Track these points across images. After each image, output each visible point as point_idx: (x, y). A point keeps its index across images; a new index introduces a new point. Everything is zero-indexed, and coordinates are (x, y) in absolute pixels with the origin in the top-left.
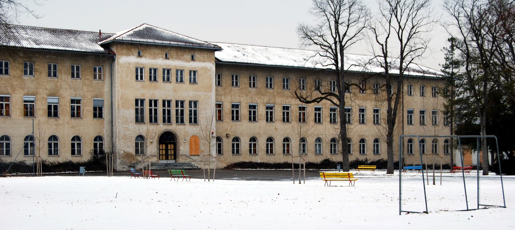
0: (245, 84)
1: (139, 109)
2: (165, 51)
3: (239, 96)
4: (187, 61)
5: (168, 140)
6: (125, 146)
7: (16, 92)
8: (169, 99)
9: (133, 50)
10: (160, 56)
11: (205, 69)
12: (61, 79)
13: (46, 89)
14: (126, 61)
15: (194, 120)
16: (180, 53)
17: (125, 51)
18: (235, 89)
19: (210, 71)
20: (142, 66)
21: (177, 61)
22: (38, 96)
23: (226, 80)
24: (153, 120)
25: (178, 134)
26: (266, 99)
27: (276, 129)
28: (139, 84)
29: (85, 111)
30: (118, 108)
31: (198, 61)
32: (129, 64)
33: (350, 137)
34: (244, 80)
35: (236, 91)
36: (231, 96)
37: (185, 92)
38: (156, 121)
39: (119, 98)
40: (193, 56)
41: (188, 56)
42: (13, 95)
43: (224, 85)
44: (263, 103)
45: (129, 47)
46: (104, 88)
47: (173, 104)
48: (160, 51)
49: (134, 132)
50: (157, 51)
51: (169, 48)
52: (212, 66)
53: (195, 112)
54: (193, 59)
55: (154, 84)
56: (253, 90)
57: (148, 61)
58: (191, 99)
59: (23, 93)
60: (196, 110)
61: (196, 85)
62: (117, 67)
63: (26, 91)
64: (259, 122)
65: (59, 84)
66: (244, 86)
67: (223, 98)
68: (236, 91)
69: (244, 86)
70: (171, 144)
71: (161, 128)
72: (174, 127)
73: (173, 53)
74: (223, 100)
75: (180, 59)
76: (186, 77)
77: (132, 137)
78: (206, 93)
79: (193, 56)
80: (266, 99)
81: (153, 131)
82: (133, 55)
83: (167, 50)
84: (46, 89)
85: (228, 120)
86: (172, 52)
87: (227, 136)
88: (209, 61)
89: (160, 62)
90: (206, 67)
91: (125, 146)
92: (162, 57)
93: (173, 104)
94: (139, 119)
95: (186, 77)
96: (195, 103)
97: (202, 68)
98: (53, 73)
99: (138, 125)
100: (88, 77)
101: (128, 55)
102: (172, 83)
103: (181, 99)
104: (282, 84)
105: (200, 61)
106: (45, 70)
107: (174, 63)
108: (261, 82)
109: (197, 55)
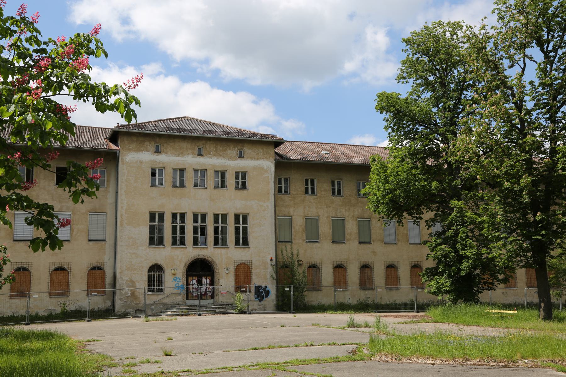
0: (325, 190)
2: (198, 144)
3: (316, 208)
4: (232, 158)
5: (200, 269)
8: (203, 211)
9: (147, 143)
10: (190, 151)
11: (260, 169)
14: (136, 160)
15: (242, 240)
16: (220, 148)
17: (133, 145)
18: (310, 198)
19: (266, 171)
20: (161, 166)
21: (216, 158)
23: (296, 184)
24: (179, 241)
25: (217, 262)
26: (357, 212)
27: (374, 253)
28: (155, 191)
29: (75, 230)
31: (248, 158)
32: (141, 162)
34: (323, 186)
35: (312, 201)
36: (305, 207)
37: (230, 202)
38: (183, 243)
40: (241, 152)
41: (152, 146)
43: (293, 192)
44: (353, 216)
45: (141, 139)
46: (107, 198)
47: (210, 219)
50: (184, 145)
51: (204, 142)
52: (269, 165)
53: (245, 230)
54: (241, 156)
55: (180, 190)
56: (337, 199)
57: (169, 159)
58: (237, 212)
60: (184, 226)
61: (246, 192)
64: (348, 243)
66: (323, 193)
67: (291, 210)
68: (312, 201)
69: (323, 193)
70: (206, 276)
71: (191, 252)
72: (210, 252)
73: (210, 147)
74: (292, 214)
75: (220, 155)
76: (230, 180)
77: (142, 267)
78: (259, 205)
79: (241, 152)
80: (357, 212)
81: (175, 260)
82: (148, 150)
83: (200, 144)
85: (300, 241)
86: (208, 146)
88: (266, 158)
89: (189, 160)
90: (262, 166)
92: (193, 153)
93: (210, 219)
94: (155, 240)
95: (230, 180)
96: (245, 218)
97: (255, 168)
99: (152, 249)
101: (138, 150)
102: (208, 190)
103: (220, 211)
104: (330, 188)
106: (327, 186)
107: (212, 161)
108: (348, 188)
109: (247, 150)
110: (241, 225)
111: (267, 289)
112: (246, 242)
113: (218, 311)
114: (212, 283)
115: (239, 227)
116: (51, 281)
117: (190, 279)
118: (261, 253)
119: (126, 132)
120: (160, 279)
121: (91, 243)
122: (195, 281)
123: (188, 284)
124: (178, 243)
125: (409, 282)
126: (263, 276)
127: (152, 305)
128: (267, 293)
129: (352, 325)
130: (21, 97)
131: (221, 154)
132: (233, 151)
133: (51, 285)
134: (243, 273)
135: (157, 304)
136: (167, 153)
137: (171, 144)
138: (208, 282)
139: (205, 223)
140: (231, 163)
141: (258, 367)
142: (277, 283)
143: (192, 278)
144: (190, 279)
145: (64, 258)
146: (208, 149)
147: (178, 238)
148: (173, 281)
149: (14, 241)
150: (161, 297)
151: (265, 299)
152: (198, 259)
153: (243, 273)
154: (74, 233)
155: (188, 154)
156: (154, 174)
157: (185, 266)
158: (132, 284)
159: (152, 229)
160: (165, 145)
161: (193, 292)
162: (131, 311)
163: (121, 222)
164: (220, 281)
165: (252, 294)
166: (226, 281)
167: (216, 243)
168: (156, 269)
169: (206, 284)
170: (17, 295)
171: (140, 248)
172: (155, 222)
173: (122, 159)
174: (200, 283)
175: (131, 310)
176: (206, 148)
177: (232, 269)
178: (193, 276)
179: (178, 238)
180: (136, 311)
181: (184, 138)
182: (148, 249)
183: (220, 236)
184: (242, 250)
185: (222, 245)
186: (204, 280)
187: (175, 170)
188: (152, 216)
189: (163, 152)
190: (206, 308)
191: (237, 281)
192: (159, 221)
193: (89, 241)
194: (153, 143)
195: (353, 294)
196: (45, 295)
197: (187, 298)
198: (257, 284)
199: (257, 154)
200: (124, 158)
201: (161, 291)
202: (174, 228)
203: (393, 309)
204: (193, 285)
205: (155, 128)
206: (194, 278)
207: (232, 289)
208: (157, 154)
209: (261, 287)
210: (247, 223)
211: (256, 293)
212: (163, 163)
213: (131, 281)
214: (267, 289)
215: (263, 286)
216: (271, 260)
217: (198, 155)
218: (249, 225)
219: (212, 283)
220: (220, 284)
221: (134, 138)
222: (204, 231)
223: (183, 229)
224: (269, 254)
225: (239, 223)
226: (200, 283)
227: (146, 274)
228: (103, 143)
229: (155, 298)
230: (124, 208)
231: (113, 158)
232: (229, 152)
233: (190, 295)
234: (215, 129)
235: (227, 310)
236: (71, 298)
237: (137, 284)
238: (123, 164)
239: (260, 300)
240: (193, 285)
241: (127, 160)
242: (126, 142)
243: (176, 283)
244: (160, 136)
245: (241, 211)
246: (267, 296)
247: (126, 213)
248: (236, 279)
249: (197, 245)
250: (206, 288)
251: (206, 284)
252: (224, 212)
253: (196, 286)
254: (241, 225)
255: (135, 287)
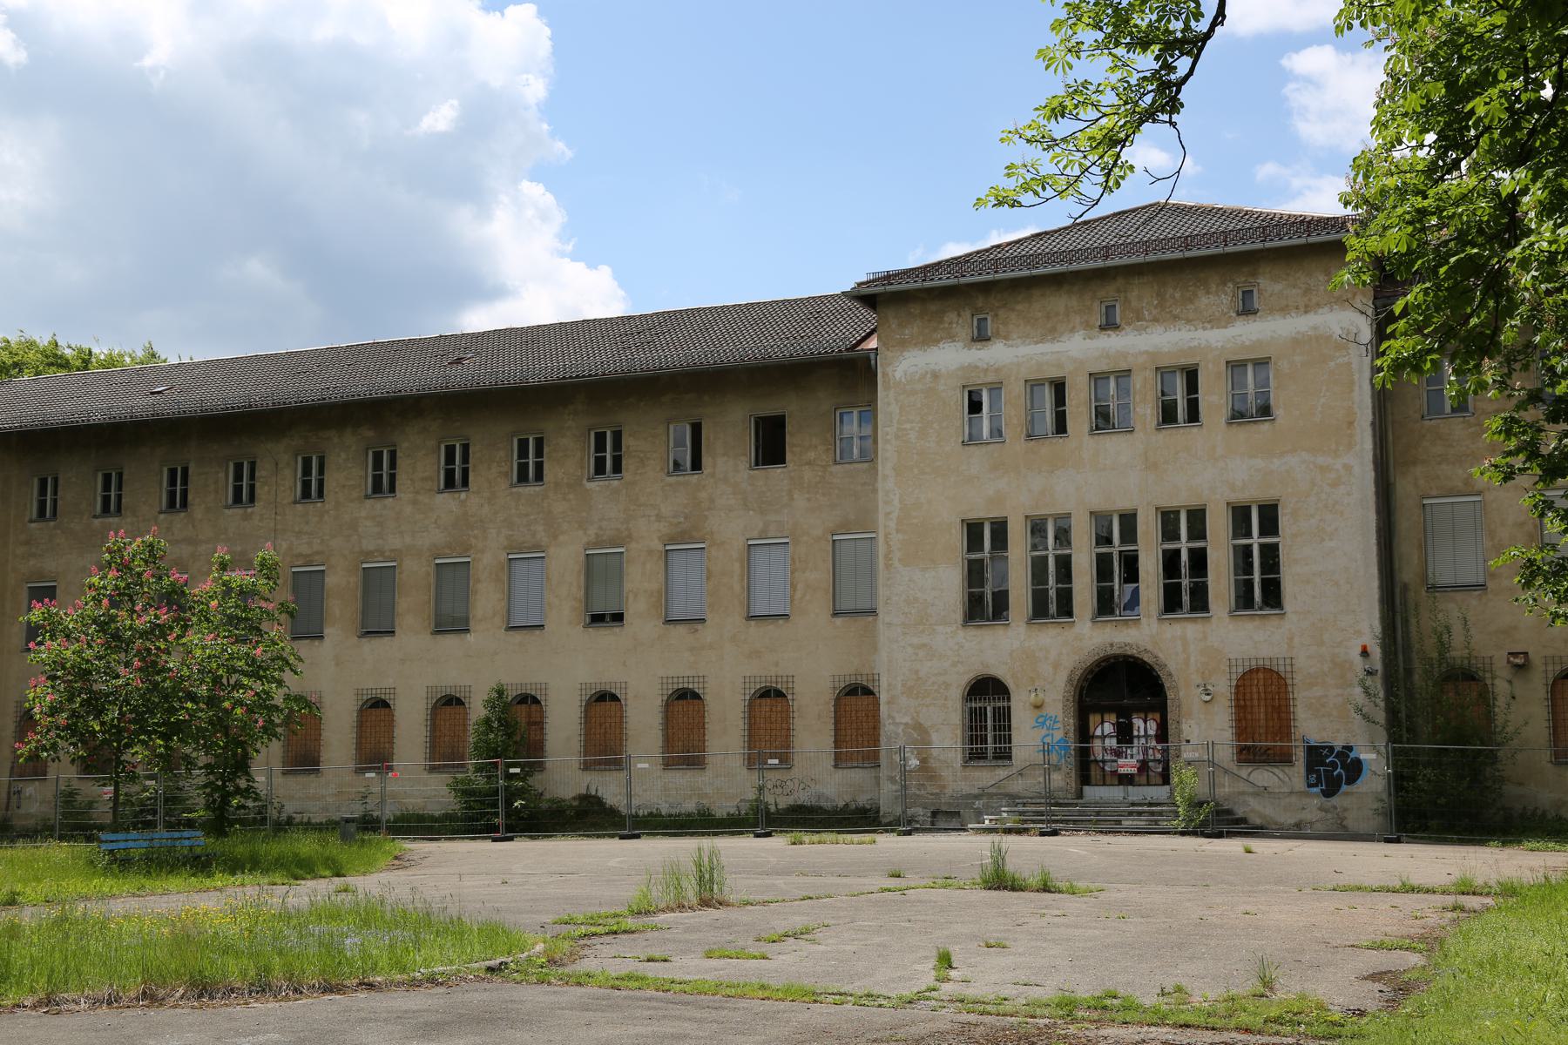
1: (1184, 556)
2: (1101, 293)
4: (1214, 322)
6: (923, 717)
7: (561, 538)
8: (1125, 504)
9: (952, 316)
10: (1077, 319)
11: (1317, 342)
12: (713, 475)
13: (659, 518)
15: (1262, 590)
17: (912, 330)
20: (991, 378)
21: (1159, 329)
22: (633, 545)
24: (1052, 604)
25: (1172, 666)
30: (888, 566)
31: (1271, 311)
32: (936, 376)
33: (1381, 819)
37: (1211, 469)
38: (1066, 609)
39: (892, 525)
41: (961, 323)
42: (552, 550)
45: (933, 307)
47: (1149, 528)
48: (1074, 302)
49: (954, 664)
50: (1059, 302)
51: (1120, 282)
53: (1271, 555)
54: (1247, 310)
57: (1017, 353)
58: (1241, 497)
59: (585, 540)
62: (886, 398)
63: (592, 531)
65: (703, 495)
70: (1145, 711)
72: (1148, 633)
73: (1141, 295)
75: (1176, 318)
77: (947, 686)
81: (1042, 660)
82: (952, 338)
83: (1109, 291)
84: (659, 518)
86: (1133, 295)
87: (1521, 666)
89: (1077, 348)
91: (923, 717)
92: (1087, 325)
93: (1149, 528)
94: (984, 606)
96: (1270, 517)
97: (1297, 342)
98: (608, 460)
100: (812, 455)
101: (927, 342)
103: (1181, 499)
105: (1284, 310)
107: (1151, 340)
109: (1269, 285)
110: (1256, 540)
111: (1352, 755)
112: (1273, 595)
113: (1127, 823)
114: (1162, 735)
115: (1251, 546)
116: (750, 725)
117: (1094, 719)
118: (1327, 626)
119: (1261, 251)
120: (1004, 718)
121: (839, 621)
122: (1108, 728)
123: (1084, 734)
124: (1053, 608)
125: (660, 743)
126: (1336, 706)
127: (977, 797)
128: (1355, 769)
129: (1000, 881)
130: (1492, 140)
131: (1177, 311)
132: (1218, 297)
133: (750, 736)
134: (1262, 701)
135: (991, 796)
136: (1006, 338)
137: (1019, 307)
138: (1152, 732)
139: (1134, 541)
140: (1205, 334)
141: (728, 991)
142: (1393, 738)
143: (1098, 718)
144: (1094, 719)
145: (777, 664)
146: (1134, 304)
147: (1052, 593)
148: (1039, 726)
149: (668, 622)
150: (1002, 773)
151: (1344, 788)
152: (1116, 657)
153: (1262, 701)
154: (798, 595)
155: (1073, 330)
156: (975, 407)
157: (1070, 680)
158: (921, 733)
159: (975, 573)
160: (1001, 313)
161: (1104, 762)
162: (919, 812)
163: (887, 557)
164: (1184, 727)
165: (1296, 774)
166: (1204, 726)
167: (1172, 602)
168: (987, 691)
169: (1146, 736)
170: (600, 762)
171: (940, 628)
172: (981, 549)
173: (884, 374)
174: (1125, 734)
175: (920, 811)
176: (1127, 300)
177: (1223, 687)
178: (1102, 710)
179: (1052, 593)
180: (935, 814)
181: (1057, 281)
182: (961, 633)
183: (1185, 582)
184: (1257, 622)
185: (1193, 609)
186: (1138, 723)
187: (1033, 385)
188: (973, 531)
189: (997, 335)
190: (1098, 813)
191: (1242, 727)
192: (993, 547)
193: (835, 614)
194: (967, 314)
195: (727, 779)
196: (737, 763)
197: (1085, 779)
198: (1316, 738)
199: (1307, 291)
200: (889, 370)
201: (1004, 755)
202: (1039, 567)
203: (682, 827)
204: (1103, 737)
205: (1033, 260)
206: (1106, 717)
207: (1226, 754)
208: (979, 345)
209: (1331, 749)
210: (1203, 537)
211: (1310, 769)
212: (997, 370)
213: (919, 727)
214: (1352, 755)
215: (1338, 743)
216: (1365, 653)
217: (1102, 328)
218: (1286, 539)
219: (1162, 735)
220: (1184, 736)
221: (915, 309)
222: (1131, 567)
223: (1064, 565)
224: (1359, 633)
225: (1249, 534)
226: (1125, 734)
227: (959, 705)
228: (832, 338)
229: (986, 776)
230: (895, 515)
231: (852, 375)
232: (1204, 301)
233: (1095, 772)
234: (1217, 225)
235: (1156, 822)
236: (795, 772)
237: (934, 737)
238: (887, 388)
239: (1329, 793)
240: (1103, 737)
241: (898, 375)
242: (894, 324)
243: (1044, 732)
244: (986, 288)
245: (1253, 494)
246: (1351, 780)
247: (898, 531)
248: (1238, 720)
249: (1112, 612)
250: (1146, 750)
251: (1146, 736)
252: (1194, 502)
253: (1112, 743)
254: (1184, 545)
255: (930, 743)
